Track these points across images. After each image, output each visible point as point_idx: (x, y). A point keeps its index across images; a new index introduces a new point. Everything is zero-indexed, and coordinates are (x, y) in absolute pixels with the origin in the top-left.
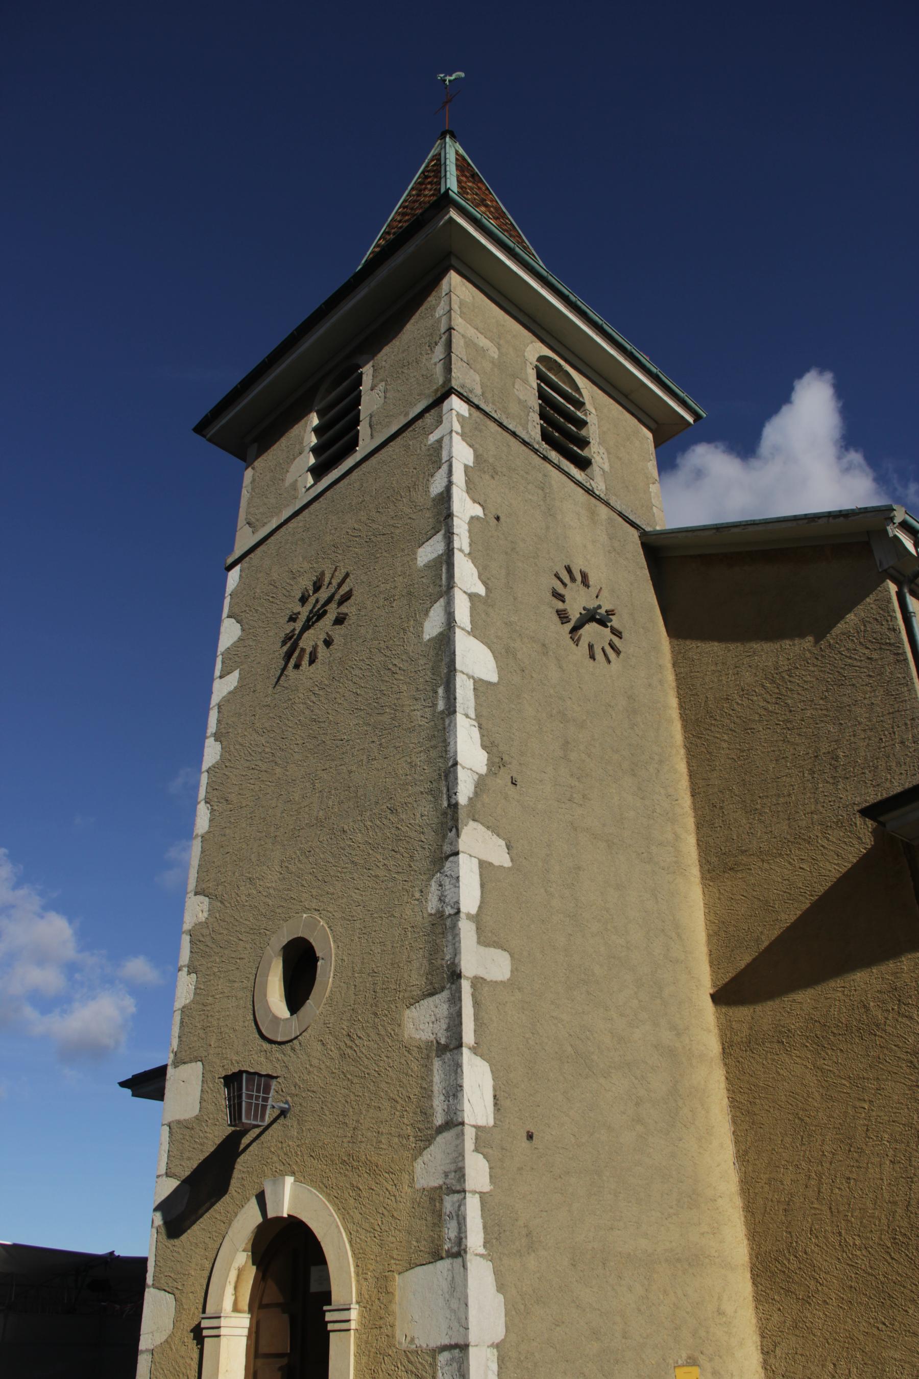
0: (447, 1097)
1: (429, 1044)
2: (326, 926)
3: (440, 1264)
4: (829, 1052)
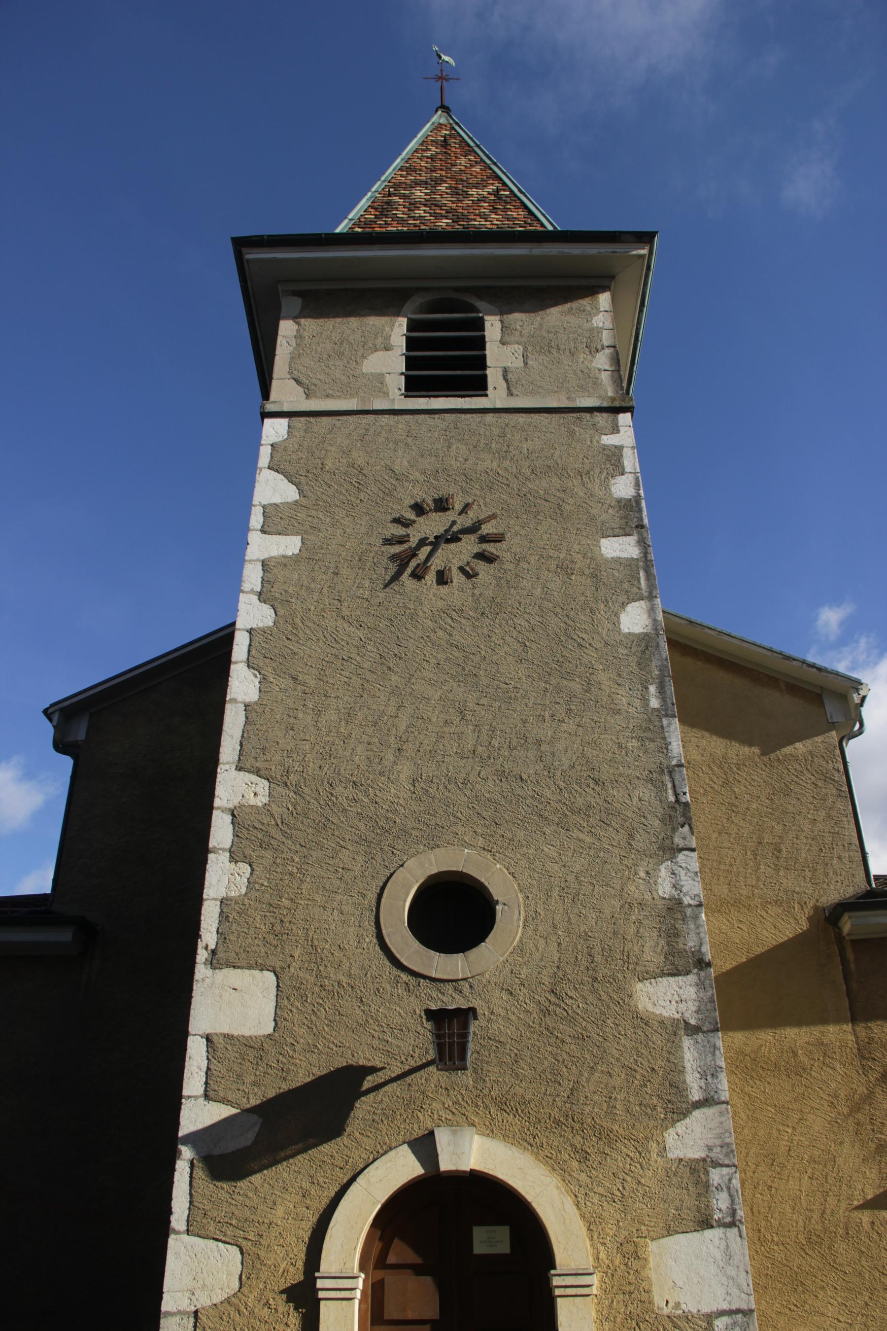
0: (703, 1075)
1: (675, 1022)
2: (502, 867)
3: (708, 1233)
4: (758, 1082)
